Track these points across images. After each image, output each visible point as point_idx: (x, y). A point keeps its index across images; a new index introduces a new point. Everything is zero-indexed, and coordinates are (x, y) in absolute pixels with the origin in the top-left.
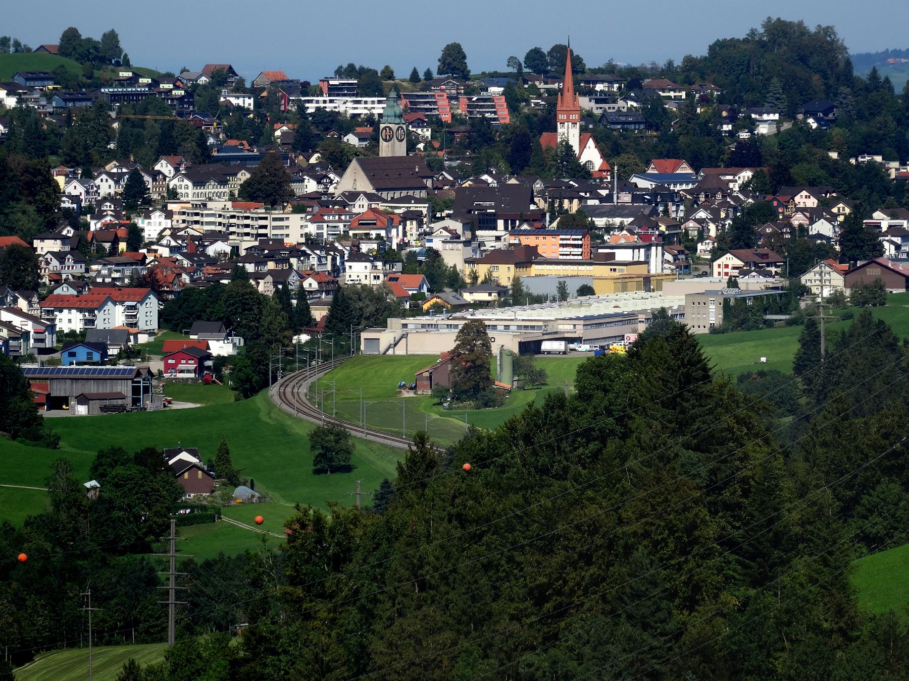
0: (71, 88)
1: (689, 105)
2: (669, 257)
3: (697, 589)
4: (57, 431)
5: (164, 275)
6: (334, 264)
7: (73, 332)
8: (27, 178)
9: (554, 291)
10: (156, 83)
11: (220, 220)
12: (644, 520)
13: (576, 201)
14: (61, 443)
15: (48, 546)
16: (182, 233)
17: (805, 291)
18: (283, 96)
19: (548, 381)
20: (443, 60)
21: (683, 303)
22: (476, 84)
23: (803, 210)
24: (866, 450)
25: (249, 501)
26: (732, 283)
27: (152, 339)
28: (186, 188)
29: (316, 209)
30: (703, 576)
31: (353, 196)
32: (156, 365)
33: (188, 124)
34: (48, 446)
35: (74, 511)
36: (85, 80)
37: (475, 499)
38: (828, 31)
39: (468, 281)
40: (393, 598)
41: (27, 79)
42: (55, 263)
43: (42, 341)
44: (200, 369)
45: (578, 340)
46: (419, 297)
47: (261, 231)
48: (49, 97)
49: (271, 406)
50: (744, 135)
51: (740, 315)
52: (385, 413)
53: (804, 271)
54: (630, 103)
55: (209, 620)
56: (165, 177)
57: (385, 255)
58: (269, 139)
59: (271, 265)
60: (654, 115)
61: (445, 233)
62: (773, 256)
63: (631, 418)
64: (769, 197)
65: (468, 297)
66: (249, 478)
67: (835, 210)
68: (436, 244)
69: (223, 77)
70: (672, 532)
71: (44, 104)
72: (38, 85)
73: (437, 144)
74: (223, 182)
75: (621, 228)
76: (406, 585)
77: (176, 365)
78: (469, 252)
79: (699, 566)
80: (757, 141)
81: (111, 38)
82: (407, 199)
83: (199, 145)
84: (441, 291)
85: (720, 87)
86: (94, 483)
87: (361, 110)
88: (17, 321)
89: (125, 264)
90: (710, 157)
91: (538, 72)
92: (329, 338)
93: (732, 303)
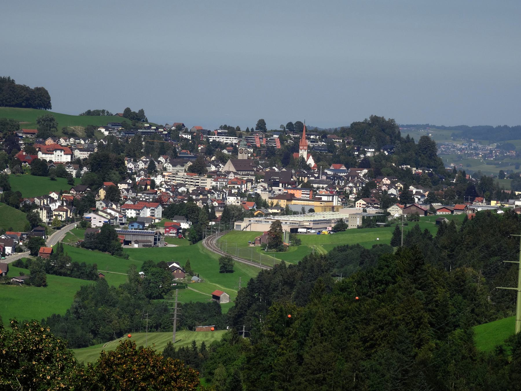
0: (128, 129)
1: (344, 144)
2: (340, 200)
3: (421, 340)
4: (128, 253)
5: (164, 198)
6: (223, 197)
7: (132, 218)
8: (116, 162)
9: (300, 210)
10: (157, 128)
11: (182, 179)
12: (403, 315)
13: (306, 178)
14: (129, 258)
15: (129, 295)
16: (169, 183)
17: (389, 214)
18: (201, 135)
19: (302, 243)
20: (258, 125)
21: (348, 217)
22: (269, 134)
23: (386, 185)
24: (450, 284)
25: (197, 282)
26: (365, 211)
27: (160, 221)
28: (169, 167)
29: (216, 177)
30: (424, 336)
31: (229, 172)
32: (162, 231)
33: (168, 144)
34: (125, 258)
35: (137, 283)
36: (132, 126)
37: (341, 304)
38: (392, 120)
39: (270, 205)
40: (312, 339)
41: (112, 125)
42: (125, 192)
43: (122, 220)
44: (178, 233)
45: (311, 228)
46: (253, 210)
47: (197, 184)
48: (120, 132)
49: (203, 247)
50: (362, 156)
51: (368, 223)
52: (246, 253)
53: (388, 207)
54: (323, 143)
55: (186, 325)
56: (162, 163)
57: (240, 194)
58: (197, 150)
59: (201, 196)
60: (331, 148)
61: (261, 187)
62: (377, 201)
63: (396, 277)
64: (374, 179)
65: (270, 211)
66: (197, 274)
67: (397, 185)
68: (259, 191)
69: (180, 127)
70: (413, 319)
71: (118, 134)
72: (116, 128)
73: (255, 155)
74: (183, 166)
75: (323, 188)
76: (317, 334)
77: (169, 231)
78: (270, 195)
79: (422, 332)
80: (366, 159)
81: (142, 112)
82: (248, 175)
83: (173, 152)
84: (260, 208)
85: (354, 139)
86: (142, 273)
87: (229, 141)
88: (113, 213)
89: (150, 194)
90: (352, 164)
91: (291, 131)
92: (223, 224)
93: (365, 218)
